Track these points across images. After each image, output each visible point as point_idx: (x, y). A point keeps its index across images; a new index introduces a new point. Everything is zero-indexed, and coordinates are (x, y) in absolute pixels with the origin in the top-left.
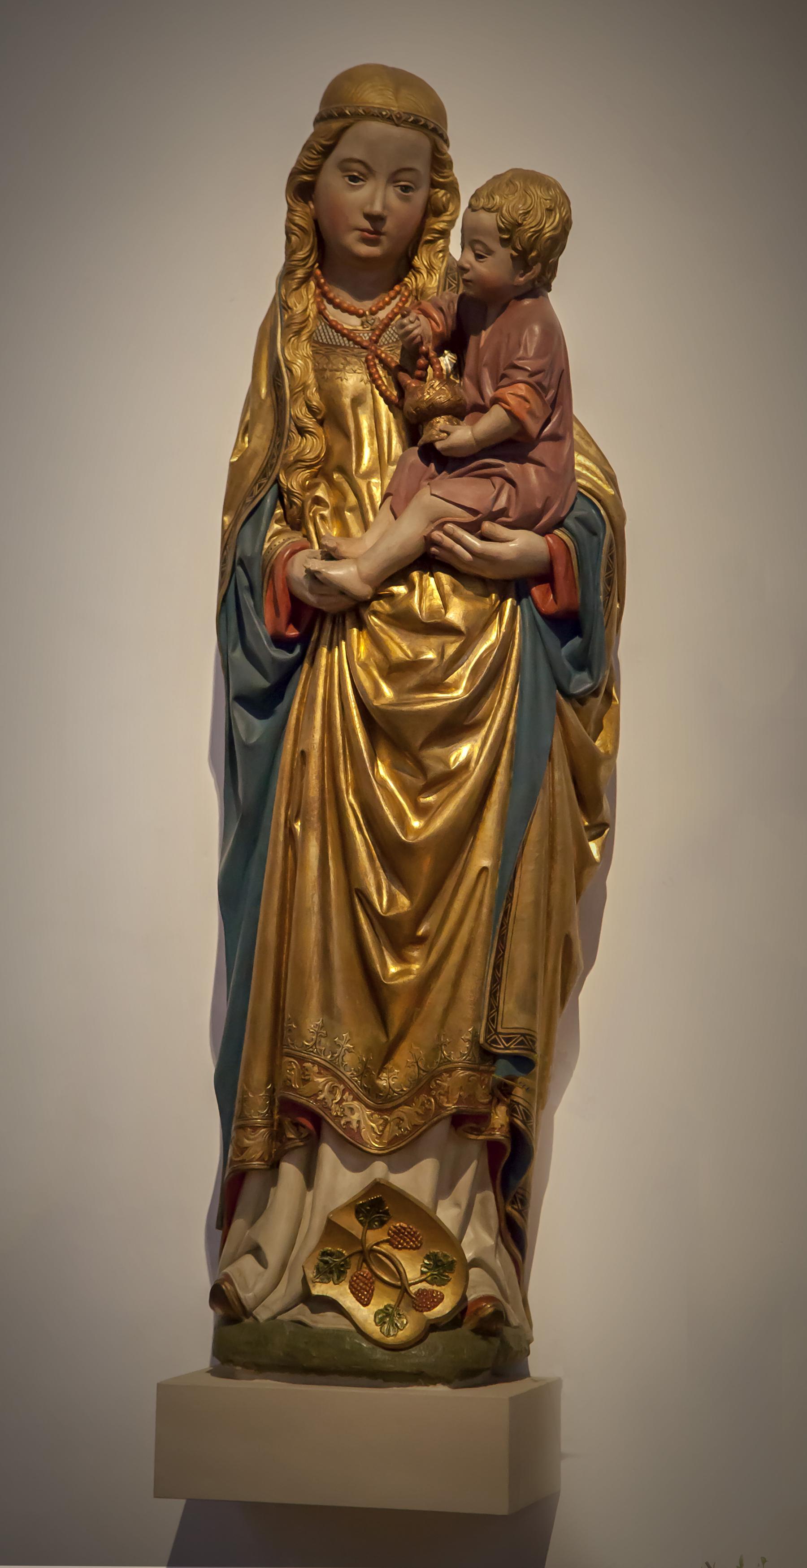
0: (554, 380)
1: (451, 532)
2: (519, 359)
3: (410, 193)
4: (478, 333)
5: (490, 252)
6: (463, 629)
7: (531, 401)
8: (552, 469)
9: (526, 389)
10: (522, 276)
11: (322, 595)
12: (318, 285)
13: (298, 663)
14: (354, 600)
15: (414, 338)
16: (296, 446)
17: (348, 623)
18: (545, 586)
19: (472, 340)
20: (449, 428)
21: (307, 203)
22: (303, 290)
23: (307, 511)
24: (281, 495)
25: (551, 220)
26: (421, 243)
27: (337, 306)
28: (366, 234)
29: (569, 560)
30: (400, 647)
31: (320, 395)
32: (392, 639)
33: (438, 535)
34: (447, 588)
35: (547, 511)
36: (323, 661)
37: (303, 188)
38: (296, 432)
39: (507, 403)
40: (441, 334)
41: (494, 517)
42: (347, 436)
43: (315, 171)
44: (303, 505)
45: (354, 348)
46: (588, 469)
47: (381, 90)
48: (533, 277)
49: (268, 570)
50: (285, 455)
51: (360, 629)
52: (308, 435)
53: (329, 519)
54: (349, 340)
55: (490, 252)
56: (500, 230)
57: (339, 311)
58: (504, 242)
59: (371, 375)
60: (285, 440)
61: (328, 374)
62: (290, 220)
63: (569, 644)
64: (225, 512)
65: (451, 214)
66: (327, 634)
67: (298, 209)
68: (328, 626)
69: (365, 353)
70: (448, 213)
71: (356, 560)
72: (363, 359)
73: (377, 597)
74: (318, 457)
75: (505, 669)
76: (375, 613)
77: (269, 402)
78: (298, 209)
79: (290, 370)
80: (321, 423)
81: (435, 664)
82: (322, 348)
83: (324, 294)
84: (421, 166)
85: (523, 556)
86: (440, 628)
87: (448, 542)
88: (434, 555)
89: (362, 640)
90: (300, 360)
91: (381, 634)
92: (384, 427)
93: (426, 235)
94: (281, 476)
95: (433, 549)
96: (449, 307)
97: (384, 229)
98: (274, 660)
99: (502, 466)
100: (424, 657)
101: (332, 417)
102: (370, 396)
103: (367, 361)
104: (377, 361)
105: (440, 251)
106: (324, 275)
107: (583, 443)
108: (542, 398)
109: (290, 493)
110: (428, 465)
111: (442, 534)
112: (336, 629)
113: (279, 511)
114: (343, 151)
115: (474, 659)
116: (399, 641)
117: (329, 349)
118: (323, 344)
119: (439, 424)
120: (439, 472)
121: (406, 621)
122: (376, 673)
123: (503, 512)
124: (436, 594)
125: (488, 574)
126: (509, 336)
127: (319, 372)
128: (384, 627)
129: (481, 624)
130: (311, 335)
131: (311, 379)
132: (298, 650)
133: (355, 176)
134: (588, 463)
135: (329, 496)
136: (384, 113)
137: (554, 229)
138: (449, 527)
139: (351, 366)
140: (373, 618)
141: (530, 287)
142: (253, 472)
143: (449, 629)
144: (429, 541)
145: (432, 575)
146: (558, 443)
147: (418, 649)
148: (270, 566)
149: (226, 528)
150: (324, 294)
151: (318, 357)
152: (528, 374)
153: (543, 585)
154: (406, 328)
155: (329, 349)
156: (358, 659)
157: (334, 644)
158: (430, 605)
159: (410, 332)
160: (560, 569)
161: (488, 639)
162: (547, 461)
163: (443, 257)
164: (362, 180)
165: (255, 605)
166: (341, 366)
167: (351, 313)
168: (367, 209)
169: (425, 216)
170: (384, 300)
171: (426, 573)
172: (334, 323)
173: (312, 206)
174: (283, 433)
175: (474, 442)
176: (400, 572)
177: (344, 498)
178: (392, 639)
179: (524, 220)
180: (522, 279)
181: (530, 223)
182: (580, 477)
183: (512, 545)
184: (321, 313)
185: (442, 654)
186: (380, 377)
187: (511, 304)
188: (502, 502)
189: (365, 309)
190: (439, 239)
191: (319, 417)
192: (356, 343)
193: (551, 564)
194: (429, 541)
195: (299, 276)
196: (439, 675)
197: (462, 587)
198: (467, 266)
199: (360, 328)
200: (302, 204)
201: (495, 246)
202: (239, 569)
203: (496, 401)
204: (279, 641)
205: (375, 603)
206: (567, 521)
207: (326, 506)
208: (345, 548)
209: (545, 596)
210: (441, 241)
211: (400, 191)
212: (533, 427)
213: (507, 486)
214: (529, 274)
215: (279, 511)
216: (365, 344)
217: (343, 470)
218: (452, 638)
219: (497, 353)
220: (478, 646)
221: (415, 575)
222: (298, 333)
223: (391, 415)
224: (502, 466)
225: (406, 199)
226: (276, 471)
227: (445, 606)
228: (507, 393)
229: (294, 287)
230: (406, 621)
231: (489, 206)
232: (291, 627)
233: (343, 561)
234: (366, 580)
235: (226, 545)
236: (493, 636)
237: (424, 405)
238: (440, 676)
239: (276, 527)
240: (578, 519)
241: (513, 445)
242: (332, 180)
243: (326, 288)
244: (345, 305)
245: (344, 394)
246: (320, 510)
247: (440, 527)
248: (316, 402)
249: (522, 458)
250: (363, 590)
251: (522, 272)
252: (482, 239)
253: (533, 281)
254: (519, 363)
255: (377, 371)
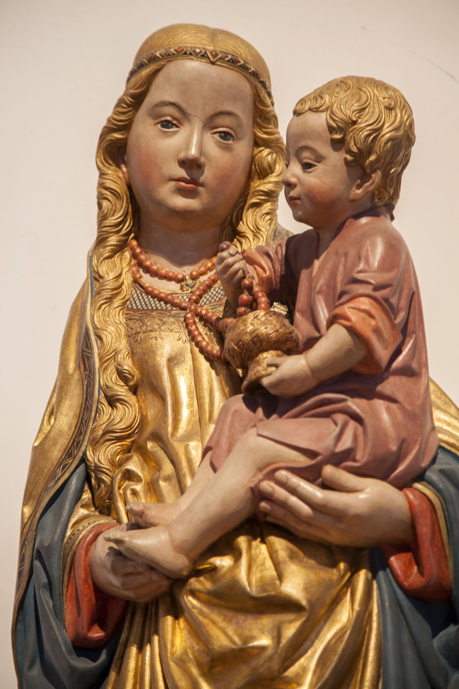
0: (404, 303)
1: (284, 480)
2: (360, 272)
3: (230, 142)
4: (309, 264)
5: (320, 159)
6: (304, 603)
7: (377, 316)
8: (408, 407)
9: (370, 303)
10: (359, 187)
11: (127, 575)
12: (134, 256)
13: (104, 673)
14: (168, 578)
15: (236, 272)
16: (105, 418)
17: (161, 611)
18: (407, 556)
19: (304, 275)
20: (278, 360)
21: (119, 166)
22: (116, 258)
23: (116, 488)
24: (90, 475)
25: (392, 119)
26: (246, 207)
27: (154, 274)
28: (183, 184)
29: (435, 521)
30: (224, 633)
31: (133, 360)
32: (214, 623)
33: (268, 486)
34: (282, 554)
35: (405, 457)
36: (132, 664)
37: (115, 149)
38: (105, 403)
39: (348, 319)
40: (269, 279)
41: (338, 459)
42: (163, 399)
43: (126, 127)
44: (112, 482)
45: (172, 310)
46: (449, 424)
47: (195, 33)
48: (372, 187)
49: (69, 560)
50: (93, 431)
51: (176, 617)
52: (118, 404)
53: (142, 494)
54: (166, 303)
55: (320, 159)
56: (331, 129)
57: (156, 279)
58: (338, 145)
59: (190, 333)
60: (93, 413)
61: (142, 335)
62: (101, 185)
63: (442, 633)
64: (25, 503)
65: (278, 176)
66: (136, 629)
67: (109, 172)
68: (138, 619)
69: (183, 313)
70: (275, 174)
71: (168, 527)
72: (182, 319)
73: (197, 573)
74: (130, 426)
75: (361, 662)
76: (193, 593)
77: (76, 376)
78: (109, 172)
79: (99, 337)
80: (134, 390)
81: (269, 652)
82: (137, 314)
83: (140, 264)
84: (243, 112)
85: (377, 513)
86: (275, 604)
87: (281, 493)
88: (266, 514)
89: (178, 631)
90: (113, 329)
91: (201, 618)
92: (205, 385)
93: (252, 198)
94: (88, 453)
95: (263, 505)
96: (276, 253)
97: (202, 179)
98: (73, 669)
99: (344, 400)
100: (256, 643)
101: (146, 382)
102: (190, 355)
103: (186, 319)
104: (197, 320)
105: (267, 214)
106: (139, 245)
107: (439, 402)
108: (391, 321)
109: (98, 469)
110: (254, 410)
111: (272, 484)
112: (148, 622)
113: (87, 496)
114: (155, 95)
115: (319, 648)
116: (222, 624)
117: (142, 312)
118: (138, 310)
119: (266, 360)
120: (268, 415)
121: (234, 600)
122: (195, 671)
123: (348, 454)
124: (269, 563)
125: (335, 536)
126: (346, 255)
127: (132, 337)
128: (205, 609)
129: (328, 601)
130: (125, 303)
131: (123, 345)
132: (103, 657)
133: (167, 121)
134: (447, 418)
135: (143, 469)
136: (198, 50)
137: (396, 129)
138: (283, 474)
139: (167, 326)
140: (190, 598)
141: (368, 205)
142: (56, 453)
143: (287, 605)
144: (257, 495)
145: (263, 541)
146: (412, 379)
147: (247, 633)
148: (71, 554)
149: (26, 521)
150: (140, 264)
151: (131, 323)
152: (371, 287)
153: (405, 555)
154: (226, 261)
155: (142, 312)
156: (172, 654)
157: (145, 641)
158: (261, 577)
159: (229, 266)
160: (424, 530)
161: (334, 622)
162: (400, 397)
163: (271, 219)
164: (177, 127)
165: (54, 606)
166: (156, 327)
167: (169, 279)
168: (182, 155)
169: (249, 177)
170: (206, 265)
171: (255, 538)
172: (150, 289)
173: (124, 169)
174: (91, 406)
175: (309, 372)
176: (222, 538)
177: (158, 467)
178: (214, 623)
179: (359, 118)
180: (359, 191)
181: (365, 123)
182: (440, 432)
183: (362, 496)
184: (136, 281)
185: (278, 637)
186: (200, 334)
187: (347, 224)
188: (346, 443)
189: (184, 274)
190: (266, 201)
191: (131, 383)
192: (174, 305)
193: (413, 525)
194: (257, 495)
195: (112, 243)
196: (275, 665)
197: (301, 554)
198: (293, 180)
199: (180, 292)
200: (114, 168)
201: (325, 149)
202: (37, 563)
203: (332, 322)
204: (82, 648)
205: (193, 580)
206: (429, 474)
207: (139, 480)
208: (154, 512)
209: (407, 567)
210: (269, 204)
211: (218, 138)
212: (382, 353)
213: (352, 424)
214: (368, 184)
215: (87, 496)
216: (184, 305)
217: (157, 437)
218: (290, 616)
219: (333, 275)
220: (325, 629)
221: (242, 541)
222: (110, 300)
223: (213, 372)
224: (344, 400)
225: (227, 148)
226: (83, 448)
227: (280, 577)
228: (347, 310)
229: (107, 255)
230: (234, 600)
231: (318, 105)
232: (96, 627)
233: (152, 529)
234: (180, 548)
235: (25, 540)
236: (345, 615)
237: (247, 338)
238: (277, 667)
239: (82, 512)
240: (442, 472)
241: (358, 375)
242: (145, 130)
243: (142, 257)
244: (163, 272)
245: (159, 353)
246: (132, 485)
247: (271, 476)
248: (129, 366)
249: (370, 394)
250: (177, 562)
251: (359, 182)
252: (309, 143)
253: (372, 195)
254: (361, 276)
255: (197, 328)
